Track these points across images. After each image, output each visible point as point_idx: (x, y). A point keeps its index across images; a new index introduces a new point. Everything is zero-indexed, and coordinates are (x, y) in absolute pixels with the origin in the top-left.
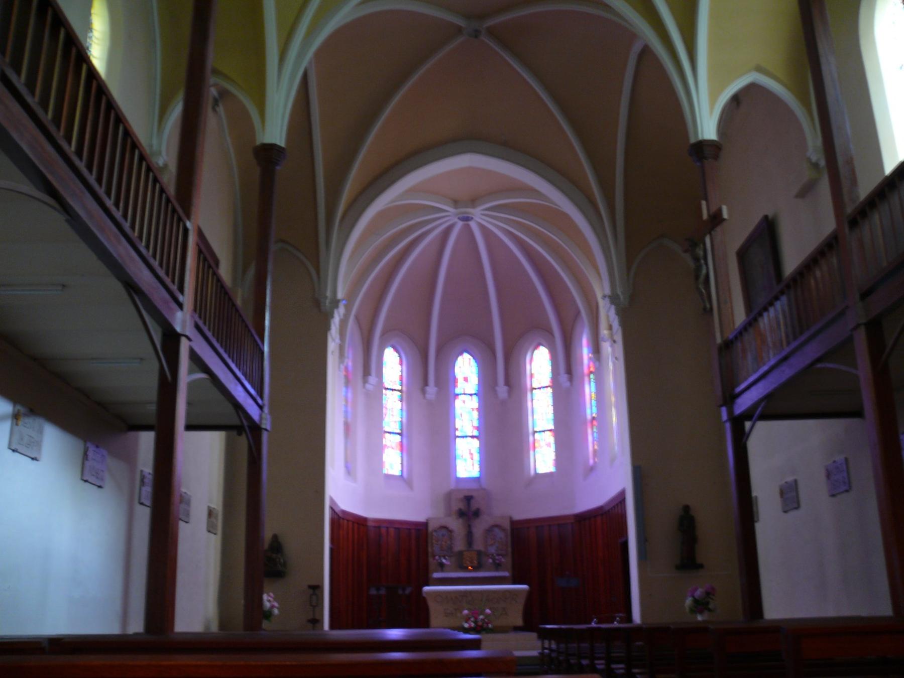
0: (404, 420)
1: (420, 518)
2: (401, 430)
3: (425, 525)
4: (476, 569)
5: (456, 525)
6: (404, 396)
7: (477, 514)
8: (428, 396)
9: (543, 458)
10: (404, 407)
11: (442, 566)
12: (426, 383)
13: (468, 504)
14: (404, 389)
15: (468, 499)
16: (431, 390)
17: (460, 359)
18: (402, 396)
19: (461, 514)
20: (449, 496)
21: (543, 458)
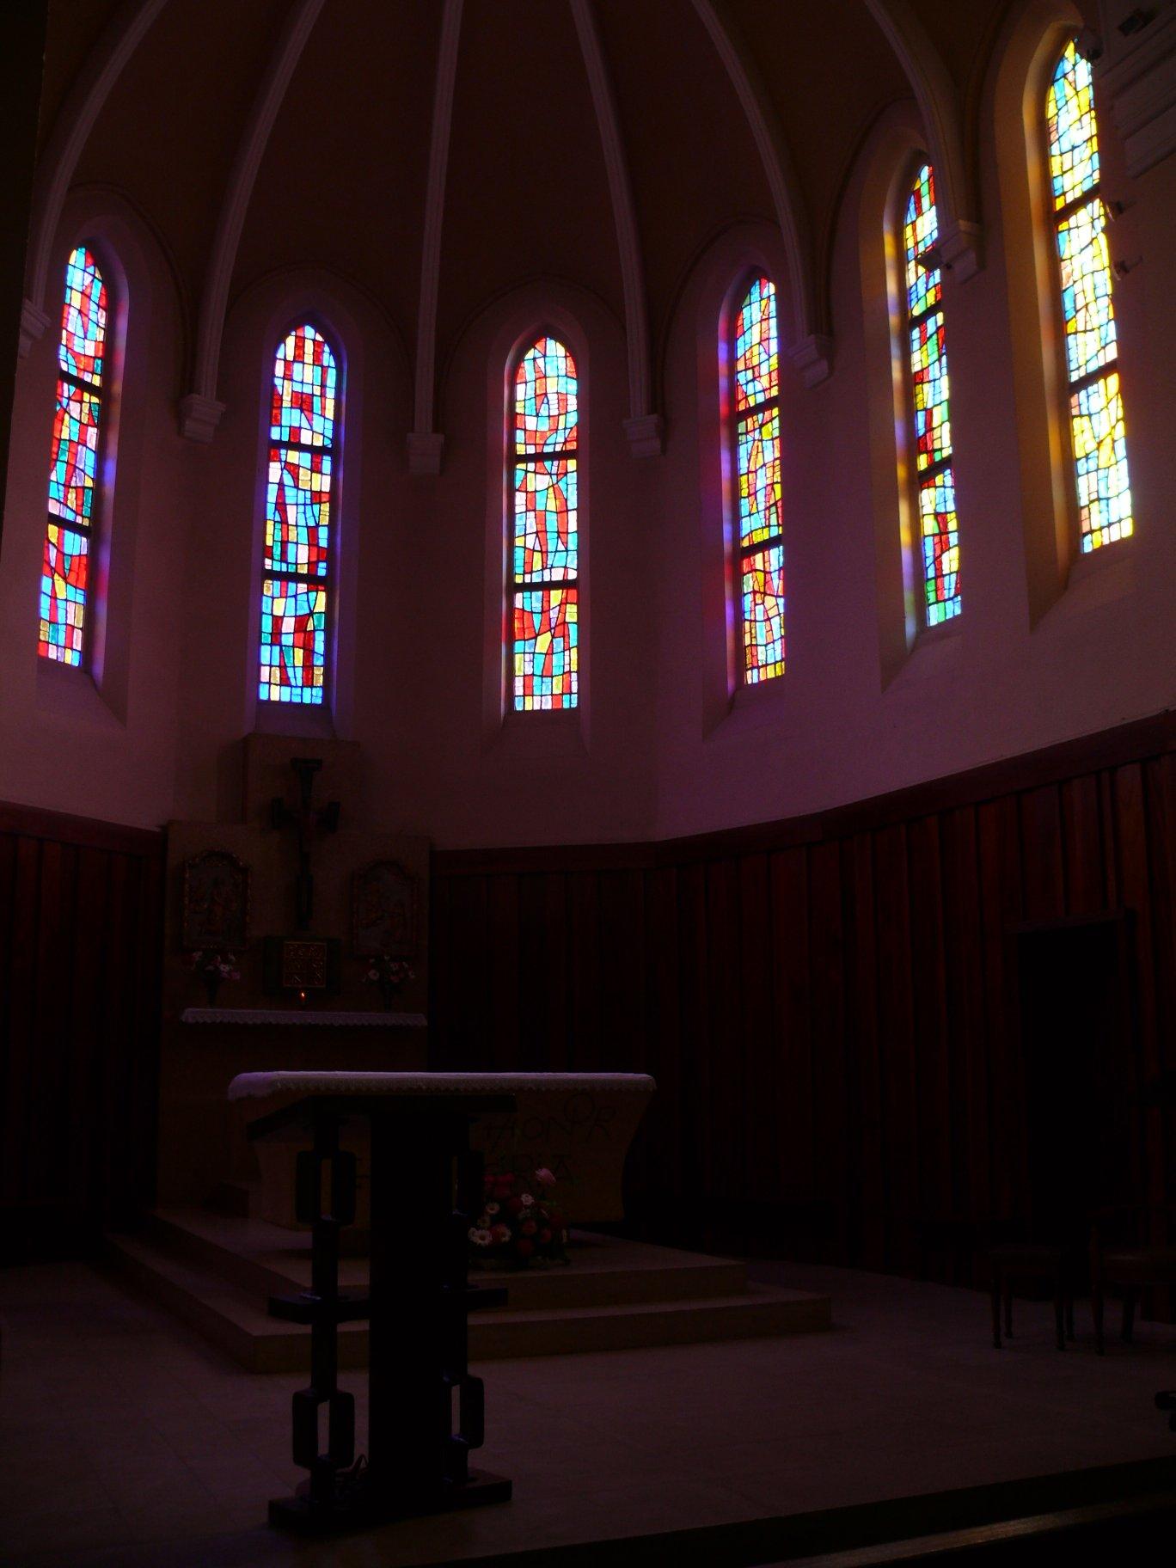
0: (109, 488)
1: (144, 818)
2: (96, 515)
6: (116, 411)
8: (189, 424)
9: (544, 671)
10: (113, 449)
12: (187, 382)
13: (291, 771)
14: (118, 388)
16: (206, 405)
17: (288, 348)
18: (104, 408)
21: (544, 671)
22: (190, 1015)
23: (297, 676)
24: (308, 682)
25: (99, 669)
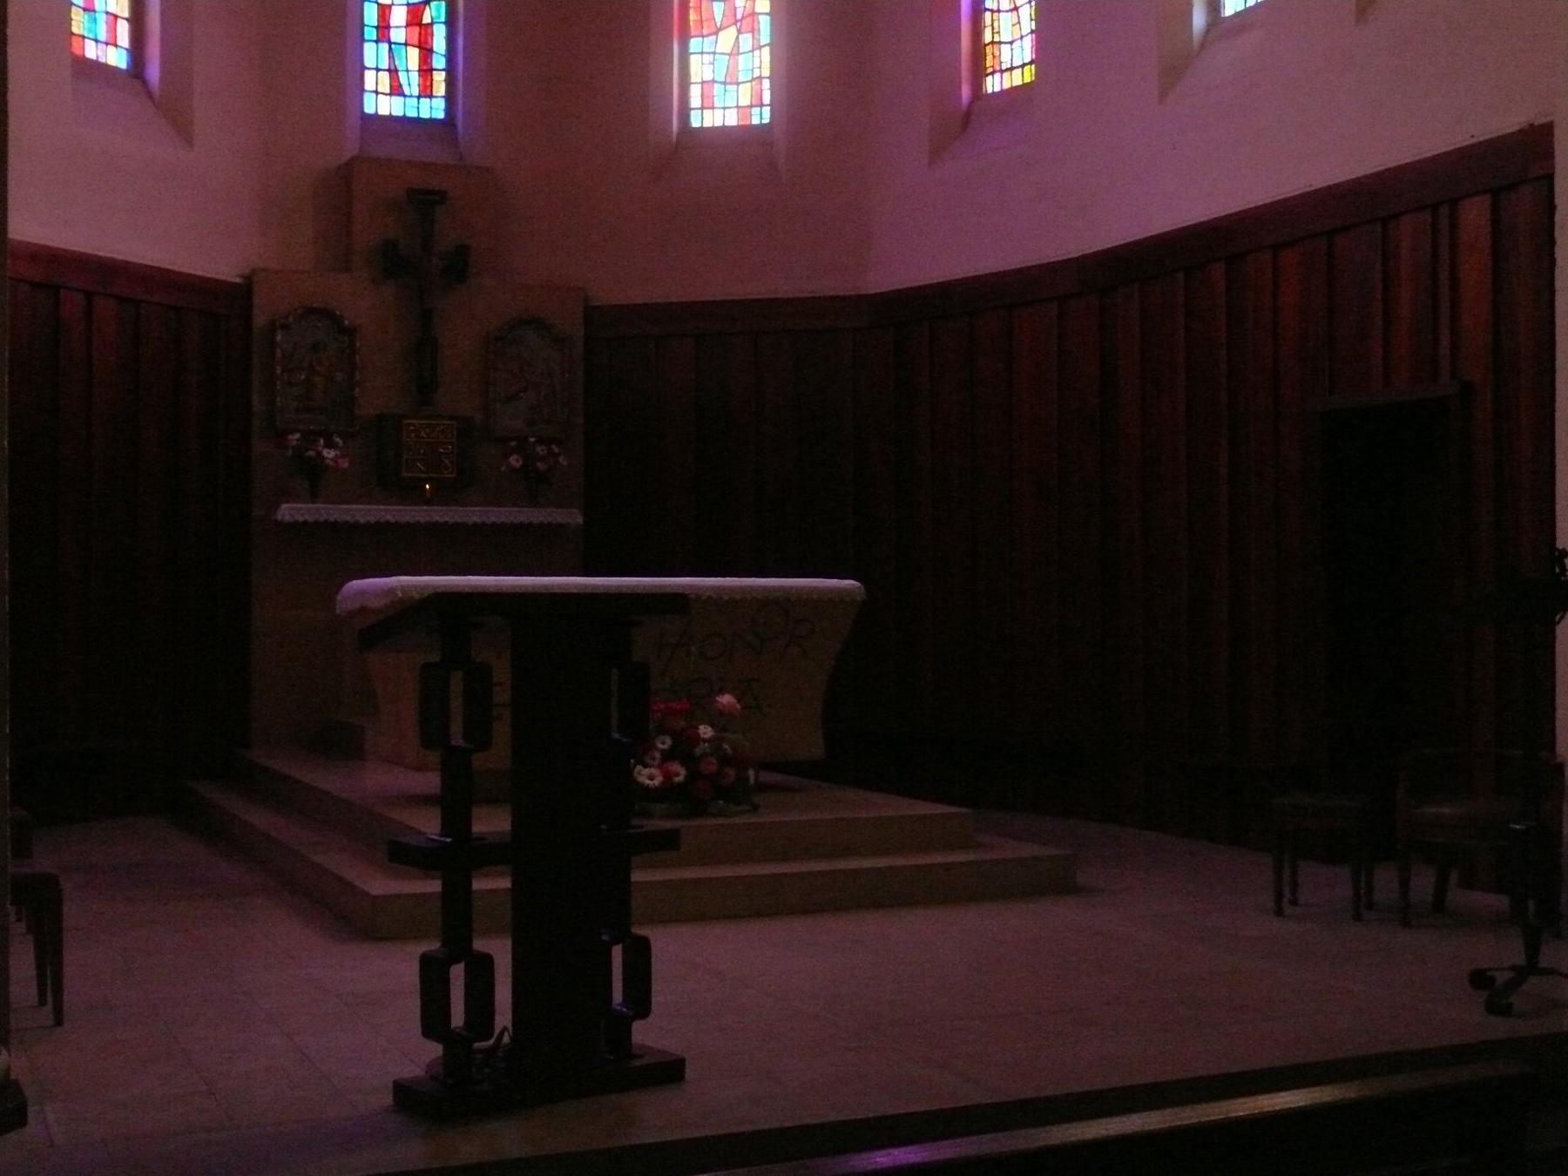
1: (223, 267)
3: (239, 295)
4: (447, 493)
5: (362, 302)
7: (458, 267)
11: (313, 477)
13: (409, 219)
15: (425, 202)
19: (393, 263)
20: (341, 185)
22: (287, 512)
23: (411, 82)
24: (426, 91)
25: (154, 72)
